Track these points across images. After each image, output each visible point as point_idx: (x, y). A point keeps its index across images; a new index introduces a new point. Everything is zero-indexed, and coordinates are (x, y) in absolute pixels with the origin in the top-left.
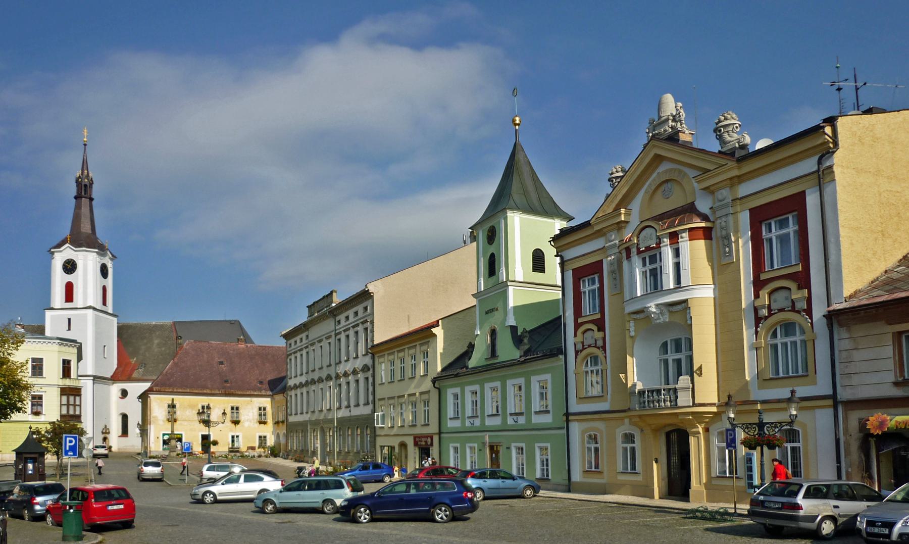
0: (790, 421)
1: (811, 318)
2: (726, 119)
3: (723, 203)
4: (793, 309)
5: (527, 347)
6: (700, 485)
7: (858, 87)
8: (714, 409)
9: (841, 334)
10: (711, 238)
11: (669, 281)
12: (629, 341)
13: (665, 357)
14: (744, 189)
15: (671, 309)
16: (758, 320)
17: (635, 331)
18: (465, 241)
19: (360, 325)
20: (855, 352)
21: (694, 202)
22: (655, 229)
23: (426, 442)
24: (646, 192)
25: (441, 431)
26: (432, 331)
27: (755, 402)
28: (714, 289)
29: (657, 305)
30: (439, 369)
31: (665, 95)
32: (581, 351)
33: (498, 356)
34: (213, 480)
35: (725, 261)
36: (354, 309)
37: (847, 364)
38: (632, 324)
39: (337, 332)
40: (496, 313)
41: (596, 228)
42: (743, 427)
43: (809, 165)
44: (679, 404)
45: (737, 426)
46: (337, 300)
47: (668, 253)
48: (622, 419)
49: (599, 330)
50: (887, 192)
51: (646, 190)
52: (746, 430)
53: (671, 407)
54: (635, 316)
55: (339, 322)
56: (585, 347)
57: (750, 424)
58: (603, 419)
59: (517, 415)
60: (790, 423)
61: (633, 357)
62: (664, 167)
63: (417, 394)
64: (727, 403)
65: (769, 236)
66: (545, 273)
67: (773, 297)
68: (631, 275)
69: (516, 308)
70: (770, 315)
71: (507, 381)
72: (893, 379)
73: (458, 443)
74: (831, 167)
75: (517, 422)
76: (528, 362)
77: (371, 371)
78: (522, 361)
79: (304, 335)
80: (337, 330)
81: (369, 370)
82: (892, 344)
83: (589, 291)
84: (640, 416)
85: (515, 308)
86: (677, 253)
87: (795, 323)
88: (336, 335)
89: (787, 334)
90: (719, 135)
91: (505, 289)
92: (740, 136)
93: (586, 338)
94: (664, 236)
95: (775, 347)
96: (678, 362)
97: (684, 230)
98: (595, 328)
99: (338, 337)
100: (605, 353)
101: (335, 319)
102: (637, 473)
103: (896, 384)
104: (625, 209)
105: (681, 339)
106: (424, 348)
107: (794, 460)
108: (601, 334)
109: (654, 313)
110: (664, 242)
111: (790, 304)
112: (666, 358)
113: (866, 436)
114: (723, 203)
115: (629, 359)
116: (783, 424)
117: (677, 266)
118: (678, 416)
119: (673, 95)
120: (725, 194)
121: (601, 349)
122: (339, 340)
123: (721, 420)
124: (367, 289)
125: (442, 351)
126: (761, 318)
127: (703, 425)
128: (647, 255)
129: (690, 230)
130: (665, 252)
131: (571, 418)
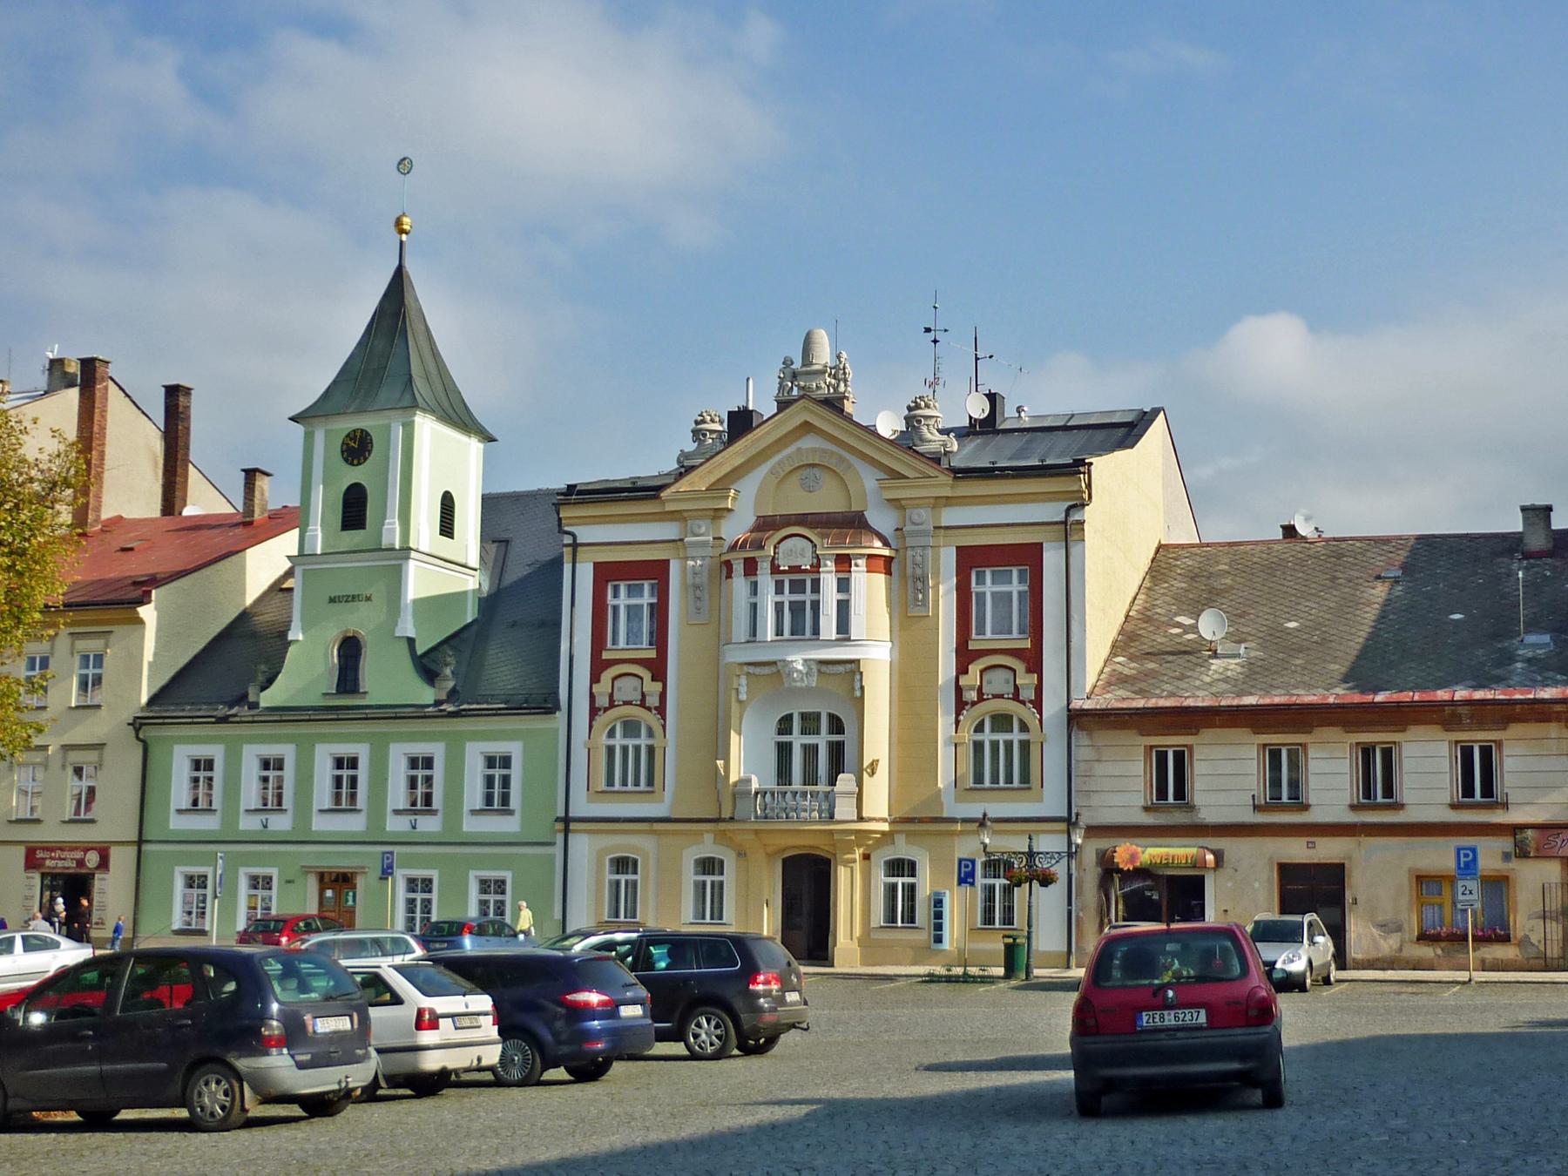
1: (1041, 713)
2: (927, 406)
3: (916, 528)
5: (451, 684)
6: (852, 939)
8: (885, 827)
9: (1080, 739)
10: (891, 574)
12: (735, 707)
14: (951, 516)
15: (824, 668)
16: (961, 705)
17: (747, 693)
20: (1096, 765)
22: (812, 542)
23: (81, 863)
24: (772, 472)
25: (144, 838)
26: (138, 613)
27: (953, 820)
28: (891, 649)
29: (805, 661)
30: (144, 699)
33: (365, 693)
35: (916, 612)
37: (1086, 779)
38: (743, 681)
40: (363, 605)
41: (670, 507)
43: (1053, 511)
44: (837, 817)
47: (829, 580)
48: (701, 833)
49: (654, 679)
51: (774, 467)
53: (820, 821)
54: (751, 669)
57: (1014, 853)
59: (415, 814)
61: (740, 734)
62: (809, 443)
63: (50, 748)
64: (907, 822)
67: (617, 683)
69: (419, 603)
70: (981, 698)
71: (317, 745)
72: (1142, 803)
74: (1082, 523)
78: (449, 712)
84: (757, 832)
85: (415, 602)
86: (844, 585)
87: (1012, 716)
93: (620, 689)
94: (826, 557)
95: (978, 747)
96: (810, 752)
97: (862, 555)
98: (646, 675)
100: (665, 720)
103: (1146, 809)
106: (91, 646)
107: (990, 906)
108: (658, 686)
109: (798, 671)
110: (826, 566)
113: (1109, 870)
114: (916, 528)
115: (734, 737)
118: (833, 834)
120: (924, 516)
121: (654, 712)
123: (703, 842)
125: (151, 659)
126: (966, 703)
127: (861, 850)
128: (787, 579)
129: (870, 556)
131: (573, 826)
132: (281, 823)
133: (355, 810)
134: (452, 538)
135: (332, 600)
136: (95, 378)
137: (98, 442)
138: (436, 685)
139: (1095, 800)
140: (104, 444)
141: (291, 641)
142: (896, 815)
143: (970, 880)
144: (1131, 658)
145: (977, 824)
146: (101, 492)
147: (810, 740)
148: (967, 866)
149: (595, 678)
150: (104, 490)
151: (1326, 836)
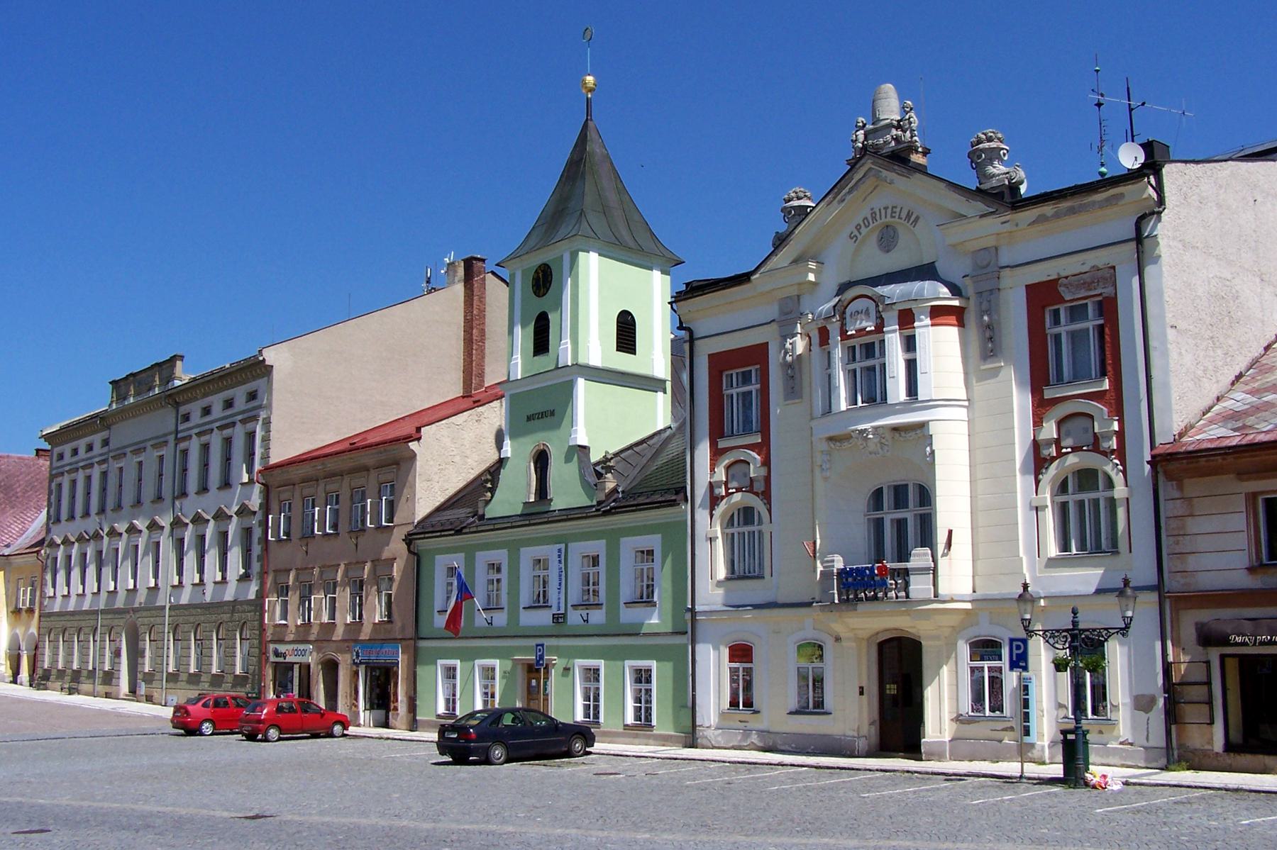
0: (1124, 626)
7: (1132, 107)
8: (968, 606)
11: (897, 390)
13: (878, 515)
18: (429, 278)
19: (239, 426)
20: (1189, 520)
21: (933, 262)
31: (883, 86)
39: (179, 436)
46: (183, 376)
47: (894, 341)
50: (1217, 279)
52: (1051, 641)
55: (186, 418)
56: (730, 491)
57: (1058, 631)
60: (1121, 629)
65: (1056, 330)
66: (635, 354)
71: (522, 549)
72: (1246, 563)
75: (587, 620)
76: (618, 513)
79: (97, 439)
80: (182, 431)
82: (1244, 510)
83: (738, 394)
86: (910, 344)
88: (178, 441)
89: (1081, 488)
90: (976, 163)
91: (570, 378)
92: (1011, 169)
96: (901, 525)
99: (182, 445)
101: (178, 411)
103: (1251, 570)
104: (817, 262)
105: (907, 485)
111: (1091, 440)
112: (881, 516)
117: (911, 366)
119: (896, 88)
122: (185, 453)
124: (261, 358)
126: (1045, 460)
130: (892, 342)
132: (500, 619)
133: (547, 606)
134: (635, 354)
135: (529, 418)
136: (473, 272)
137: (477, 322)
139: (1192, 563)
140: (484, 323)
142: (980, 593)
144: (1250, 393)
145: (1118, 593)
146: (484, 362)
147: (900, 515)
148: (540, 650)
150: (487, 360)
151: (1203, 608)
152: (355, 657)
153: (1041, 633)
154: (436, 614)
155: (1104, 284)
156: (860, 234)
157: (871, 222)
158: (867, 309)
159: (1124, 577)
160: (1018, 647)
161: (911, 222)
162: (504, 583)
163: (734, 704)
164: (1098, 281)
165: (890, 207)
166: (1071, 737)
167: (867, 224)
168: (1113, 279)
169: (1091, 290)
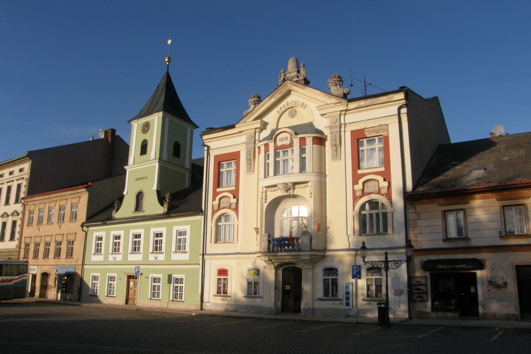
4: (379, 193)
19: (15, 181)
20: (418, 221)
21: (312, 122)
32: (361, 197)
34: (421, 291)
36: (21, 166)
42: (373, 264)
45: (368, 263)
58: (236, 259)
59: (157, 254)
68: (336, 155)
72: (442, 238)
73: (116, 273)
77: (20, 216)
81: (18, 214)
93: (223, 203)
98: (231, 196)
102: (114, 297)
108: (386, 184)
116: (403, 262)
138: (164, 206)
141: (290, 236)
143: (358, 276)
148: (137, 269)
149: (214, 199)
152: (56, 272)
153: (371, 263)
154: (92, 255)
155: (384, 131)
156: (282, 111)
157: (286, 107)
158: (287, 137)
159: (363, 241)
160: (356, 269)
161: (303, 107)
162: (103, 245)
163: (219, 292)
164: (381, 130)
165: (295, 102)
166: (383, 306)
167: (284, 106)
168: (387, 129)
169: (378, 133)
